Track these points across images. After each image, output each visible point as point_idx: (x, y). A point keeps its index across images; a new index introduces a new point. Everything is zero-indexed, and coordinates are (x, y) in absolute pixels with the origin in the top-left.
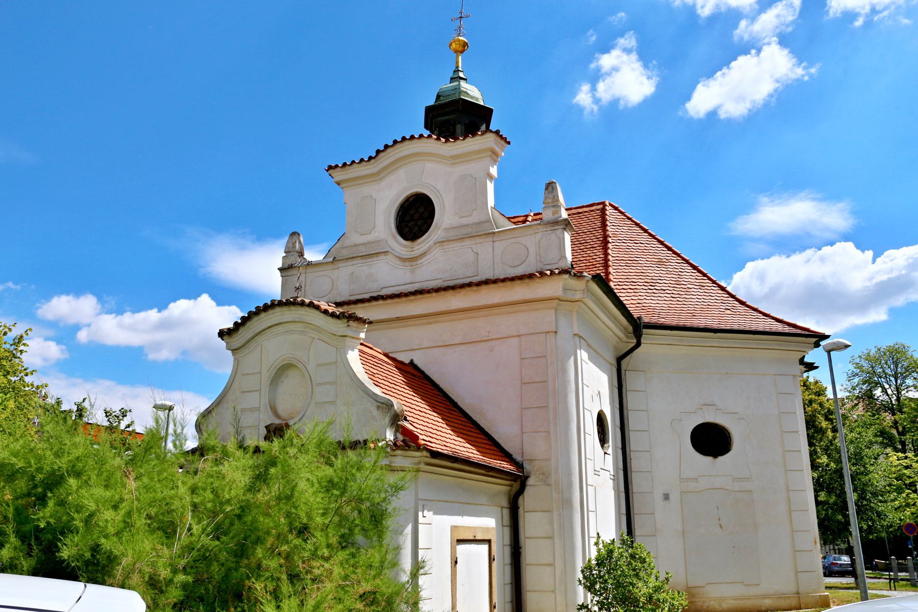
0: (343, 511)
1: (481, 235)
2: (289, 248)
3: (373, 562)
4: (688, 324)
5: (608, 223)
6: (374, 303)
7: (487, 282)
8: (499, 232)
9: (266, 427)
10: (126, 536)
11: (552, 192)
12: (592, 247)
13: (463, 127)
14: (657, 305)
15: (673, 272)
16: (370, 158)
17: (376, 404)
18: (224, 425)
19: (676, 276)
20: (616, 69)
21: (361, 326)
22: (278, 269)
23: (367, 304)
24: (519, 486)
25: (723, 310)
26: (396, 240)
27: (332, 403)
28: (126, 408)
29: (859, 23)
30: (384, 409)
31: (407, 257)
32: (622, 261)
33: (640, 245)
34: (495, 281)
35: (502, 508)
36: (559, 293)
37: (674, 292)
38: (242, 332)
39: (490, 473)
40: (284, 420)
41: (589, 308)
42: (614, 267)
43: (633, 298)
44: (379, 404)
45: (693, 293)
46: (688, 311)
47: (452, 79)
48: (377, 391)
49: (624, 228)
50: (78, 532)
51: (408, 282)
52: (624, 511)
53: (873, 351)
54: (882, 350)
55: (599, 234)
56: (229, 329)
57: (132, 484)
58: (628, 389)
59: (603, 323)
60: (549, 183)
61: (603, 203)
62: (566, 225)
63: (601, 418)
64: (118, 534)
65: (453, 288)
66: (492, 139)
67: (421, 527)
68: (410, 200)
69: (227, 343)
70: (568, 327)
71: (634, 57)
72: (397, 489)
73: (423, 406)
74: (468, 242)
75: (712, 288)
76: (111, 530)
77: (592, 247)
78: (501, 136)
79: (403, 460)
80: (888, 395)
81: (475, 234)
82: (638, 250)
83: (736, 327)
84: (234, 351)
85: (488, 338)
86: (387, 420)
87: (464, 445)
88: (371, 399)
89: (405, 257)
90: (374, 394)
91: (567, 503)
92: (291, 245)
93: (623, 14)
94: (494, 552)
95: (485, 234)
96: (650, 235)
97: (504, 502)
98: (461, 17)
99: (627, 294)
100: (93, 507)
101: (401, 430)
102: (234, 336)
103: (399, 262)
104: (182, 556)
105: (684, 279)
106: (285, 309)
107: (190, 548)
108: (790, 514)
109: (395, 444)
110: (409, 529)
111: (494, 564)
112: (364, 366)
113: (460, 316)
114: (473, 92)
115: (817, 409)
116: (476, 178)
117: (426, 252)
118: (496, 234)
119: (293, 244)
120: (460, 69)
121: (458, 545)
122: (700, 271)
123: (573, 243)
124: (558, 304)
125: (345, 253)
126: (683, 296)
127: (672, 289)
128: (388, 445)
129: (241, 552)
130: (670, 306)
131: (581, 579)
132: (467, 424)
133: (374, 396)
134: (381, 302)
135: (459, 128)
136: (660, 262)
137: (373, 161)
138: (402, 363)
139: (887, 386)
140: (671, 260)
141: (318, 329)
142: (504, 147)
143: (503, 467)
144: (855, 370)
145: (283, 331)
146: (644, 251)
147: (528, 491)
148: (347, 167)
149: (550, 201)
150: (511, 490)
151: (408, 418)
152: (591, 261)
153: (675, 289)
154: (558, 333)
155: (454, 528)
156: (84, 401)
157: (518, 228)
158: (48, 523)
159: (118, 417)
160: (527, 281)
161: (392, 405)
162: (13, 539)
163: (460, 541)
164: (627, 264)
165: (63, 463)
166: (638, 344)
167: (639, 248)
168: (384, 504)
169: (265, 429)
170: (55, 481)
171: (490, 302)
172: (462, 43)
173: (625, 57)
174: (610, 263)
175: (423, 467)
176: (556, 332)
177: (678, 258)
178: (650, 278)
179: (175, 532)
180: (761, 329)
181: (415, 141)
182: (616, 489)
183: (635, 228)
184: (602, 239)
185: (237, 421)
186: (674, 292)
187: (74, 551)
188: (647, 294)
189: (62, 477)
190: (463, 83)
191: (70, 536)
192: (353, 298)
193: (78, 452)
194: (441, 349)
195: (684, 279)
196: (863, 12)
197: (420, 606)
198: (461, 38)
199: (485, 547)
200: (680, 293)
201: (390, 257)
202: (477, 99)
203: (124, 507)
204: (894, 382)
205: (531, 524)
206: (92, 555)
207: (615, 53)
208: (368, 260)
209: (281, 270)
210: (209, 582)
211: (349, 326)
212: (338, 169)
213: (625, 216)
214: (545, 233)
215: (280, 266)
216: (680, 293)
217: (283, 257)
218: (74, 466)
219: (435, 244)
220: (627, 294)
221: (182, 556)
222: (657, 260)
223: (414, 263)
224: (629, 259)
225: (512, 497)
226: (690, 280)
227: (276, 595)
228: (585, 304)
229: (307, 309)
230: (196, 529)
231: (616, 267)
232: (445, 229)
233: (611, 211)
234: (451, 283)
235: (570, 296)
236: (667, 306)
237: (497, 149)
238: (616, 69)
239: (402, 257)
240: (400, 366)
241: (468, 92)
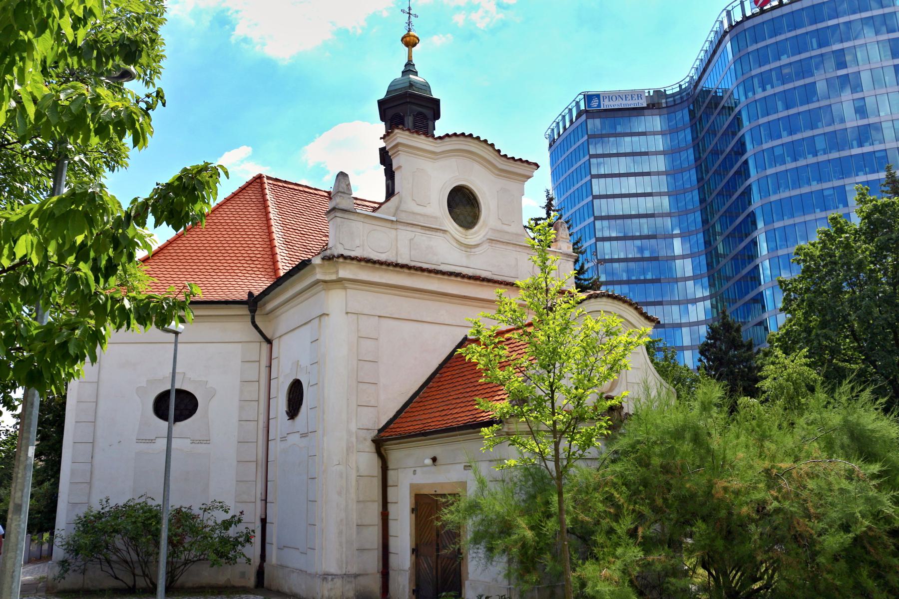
7: (403, 266)
39: (429, 437)
103: (458, 246)
106: (610, 300)
108: (94, 440)
134: (459, 279)
192: (412, 264)
197: (847, 546)
208: (428, 232)
223: (469, 250)
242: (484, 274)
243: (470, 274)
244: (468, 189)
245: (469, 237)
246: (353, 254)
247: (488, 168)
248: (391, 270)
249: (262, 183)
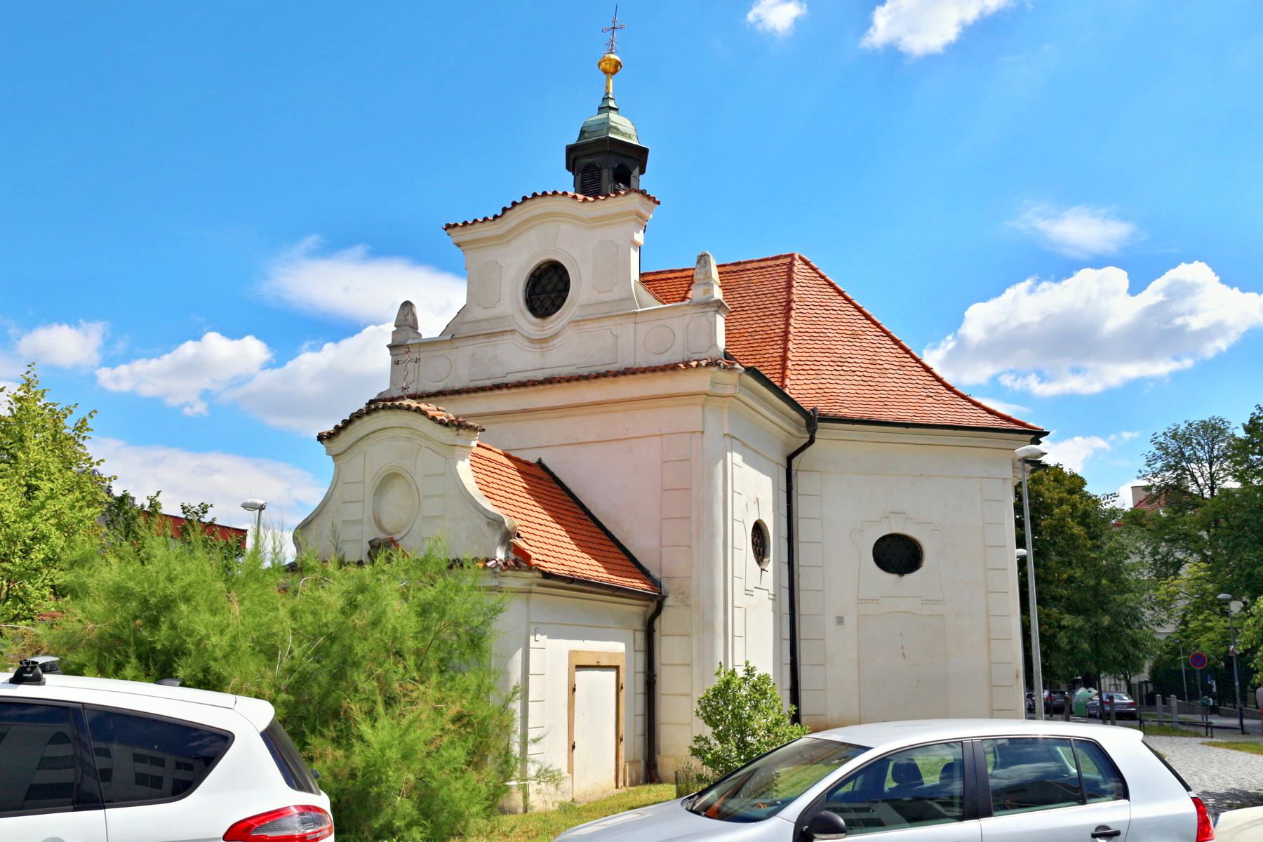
0: (442, 635)
1: (621, 315)
3: (468, 686)
4: (875, 417)
5: (795, 284)
6: (497, 392)
8: (642, 312)
9: (370, 542)
10: (232, 658)
11: (704, 267)
12: (772, 314)
13: (611, 173)
14: (842, 391)
15: (868, 348)
16: (496, 217)
17: (486, 520)
18: (319, 542)
19: (871, 354)
21: (472, 434)
22: (388, 346)
23: (489, 393)
24: (655, 607)
25: (923, 398)
26: (525, 318)
27: (442, 517)
28: (206, 503)
31: (537, 338)
32: (806, 334)
33: (832, 312)
35: (635, 630)
36: (707, 388)
37: (866, 374)
40: (389, 534)
41: (744, 403)
42: (795, 342)
43: (814, 381)
45: (889, 375)
46: (880, 399)
47: (601, 109)
48: (487, 505)
49: (814, 289)
50: (190, 655)
51: (538, 367)
52: (787, 635)
53: (1183, 426)
54: (1194, 426)
55: (782, 297)
56: (329, 433)
57: (236, 608)
58: (799, 492)
59: (766, 418)
60: (702, 256)
61: (791, 256)
62: (719, 307)
63: (759, 529)
64: (226, 657)
65: (587, 378)
66: (637, 200)
67: (532, 652)
69: (327, 448)
70: (717, 423)
72: (495, 611)
73: (545, 517)
74: (606, 323)
75: (915, 369)
76: (219, 653)
77: (772, 314)
78: (649, 197)
79: (514, 581)
80: (1199, 486)
82: (828, 319)
83: (933, 421)
84: (336, 457)
85: (625, 437)
86: (497, 538)
87: (587, 561)
88: (481, 515)
89: (534, 337)
90: (485, 509)
91: (709, 627)
92: (402, 318)
94: (622, 680)
95: (627, 314)
96: (846, 299)
97: (639, 624)
98: (614, 28)
99: (807, 377)
100: (203, 632)
101: (513, 548)
103: (527, 343)
104: (284, 677)
105: (881, 358)
107: (291, 671)
108: (989, 643)
109: (505, 564)
110: (518, 656)
111: (622, 693)
112: (477, 475)
113: (595, 409)
114: (625, 128)
115: (1067, 511)
116: (618, 246)
117: (558, 333)
118: (639, 315)
120: (610, 96)
121: (577, 671)
122: (902, 347)
123: (728, 332)
124: (705, 399)
125: (465, 330)
126: (876, 380)
127: (864, 370)
128: (497, 565)
129: (338, 676)
130: (858, 391)
131: (699, 710)
132: (599, 536)
133: (484, 512)
134: (505, 391)
136: (854, 335)
137: (498, 220)
138: (527, 464)
139: (1197, 474)
140: (868, 333)
141: (426, 437)
142: (653, 208)
143: (634, 587)
144: (1157, 452)
146: (835, 320)
147: (666, 613)
148: (468, 227)
149: (702, 277)
150: (646, 612)
151: (522, 534)
152: (769, 332)
153: (868, 370)
154: (705, 434)
155: (572, 653)
156: (158, 495)
157: (667, 308)
158: (164, 645)
159: (197, 513)
160: (669, 373)
161: (503, 522)
162: (133, 660)
163: (579, 667)
164: (812, 338)
165: (174, 589)
166: (811, 441)
167: (830, 316)
168: (483, 628)
169: (368, 545)
170: (167, 604)
171: (629, 396)
172: (614, 63)
174: (791, 336)
175: (535, 588)
176: (703, 432)
177: (878, 330)
178: (839, 355)
179: (277, 654)
180: (964, 424)
181: (547, 198)
182: (777, 611)
183: (828, 290)
184: (784, 304)
185: (335, 535)
186: (866, 374)
187: (189, 671)
188: (832, 377)
189: (174, 601)
190: (613, 115)
191: (184, 658)
192: (472, 385)
193: (188, 579)
194: (573, 447)
195: (881, 358)
198: (612, 56)
199: (613, 674)
200: (874, 375)
202: (629, 137)
203: (230, 632)
204: (1208, 469)
205: (667, 649)
206: (204, 675)
208: (493, 339)
209: (389, 346)
210: (310, 703)
211: (458, 434)
212: (458, 229)
213: (817, 273)
215: (390, 342)
216: (874, 375)
217: (394, 332)
218: (185, 592)
219: (569, 323)
220: (807, 377)
221: (284, 677)
222: (850, 332)
223: (544, 345)
224: (816, 330)
225: (647, 619)
226: (888, 358)
227: (371, 714)
228: (738, 399)
229: (414, 414)
230: (296, 653)
231: (798, 342)
232: (582, 306)
233: (799, 267)
234: (585, 372)
235: (719, 390)
236: (854, 392)
237: (643, 211)
239: (530, 337)
240: (524, 468)
241: (619, 127)
242: (564, 372)
243: (662, 364)
245: (547, 328)
247: (611, 224)
249: (791, 265)
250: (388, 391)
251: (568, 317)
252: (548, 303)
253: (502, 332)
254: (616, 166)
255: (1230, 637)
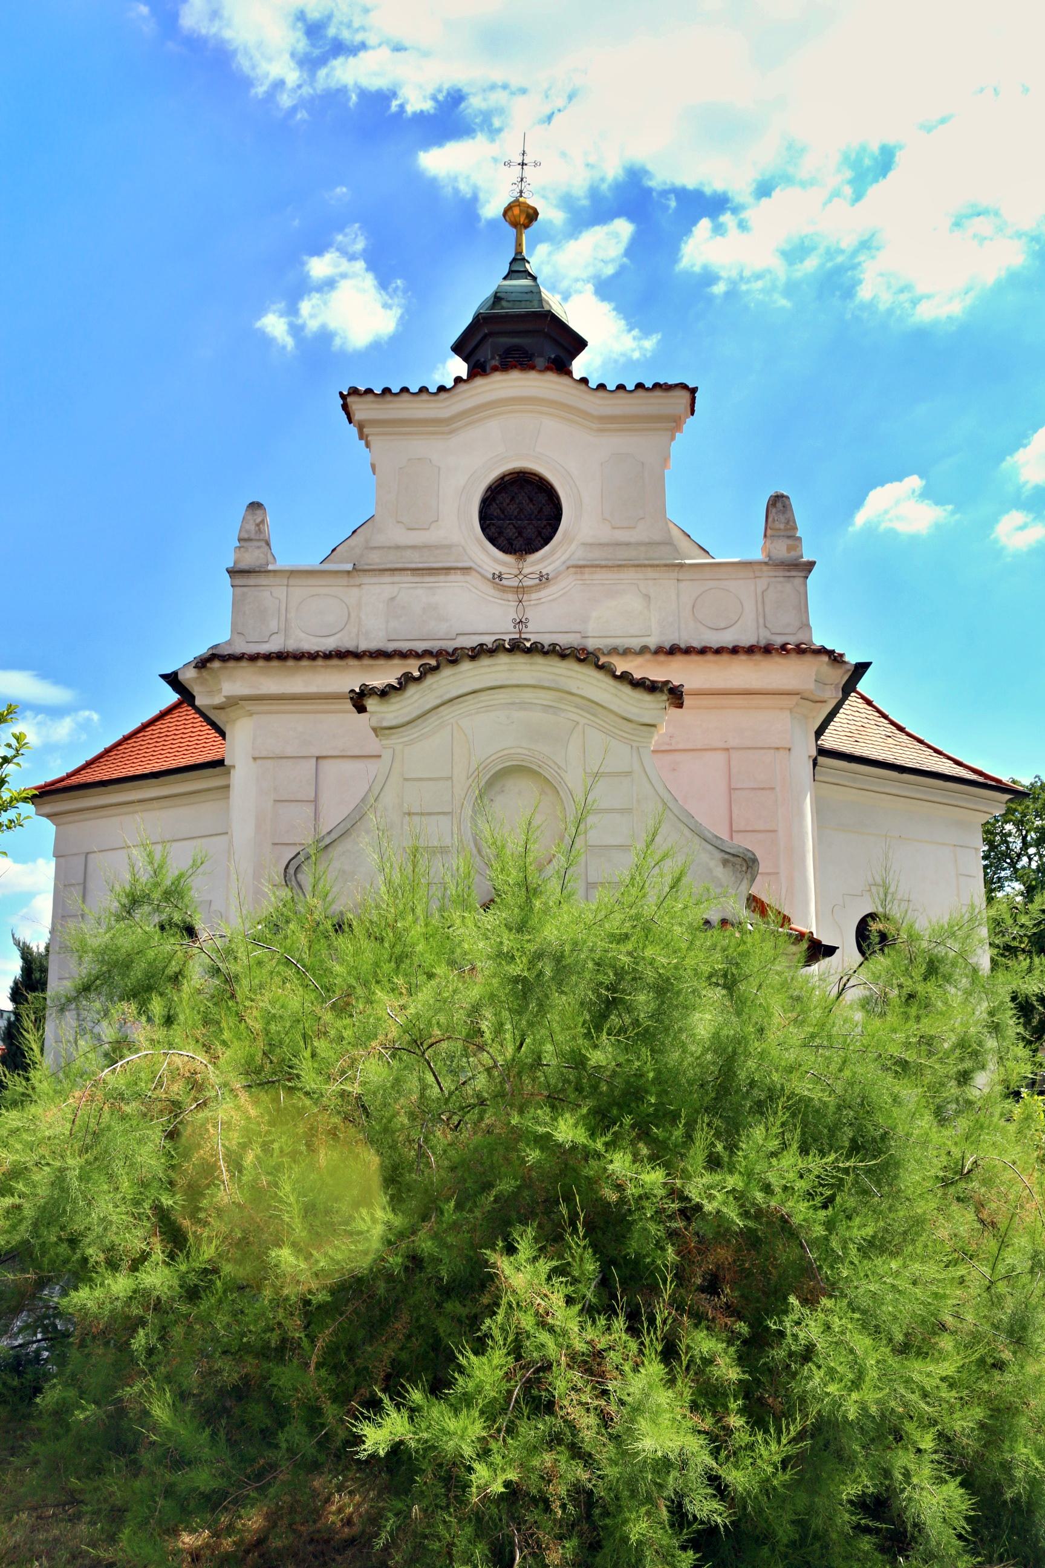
1: (657, 566)
2: (248, 532)
8: (691, 565)
17: (719, 855)
20: (330, 284)
29: (719, 289)
30: (738, 866)
34: (688, 651)
38: (412, 696)
44: (726, 856)
68: (507, 478)
71: (360, 265)
81: (647, 562)
88: (710, 847)
92: (252, 527)
93: (344, 189)
95: (666, 565)
102: (393, 700)
119: (258, 525)
125: (375, 559)
135: (540, 362)
137: (443, 395)
145: (503, 701)
149: (782, 526)
154: (792, 751)
173: (345, 265)
192: (391, 647)
196: (724, 274)
201: (472, 579)
207: (330, 257)
208: (427, 579)
214: (774, 579)
215: (230, 564)
238: (330, 284)
244: (535, 475)
246: (264, 648)
248: (322, 666)
250: (229, 643)
251: (563, 558)
252: (530, 532)
253: (448, 570)
254: (553, 356)
255: (606, 1144)
